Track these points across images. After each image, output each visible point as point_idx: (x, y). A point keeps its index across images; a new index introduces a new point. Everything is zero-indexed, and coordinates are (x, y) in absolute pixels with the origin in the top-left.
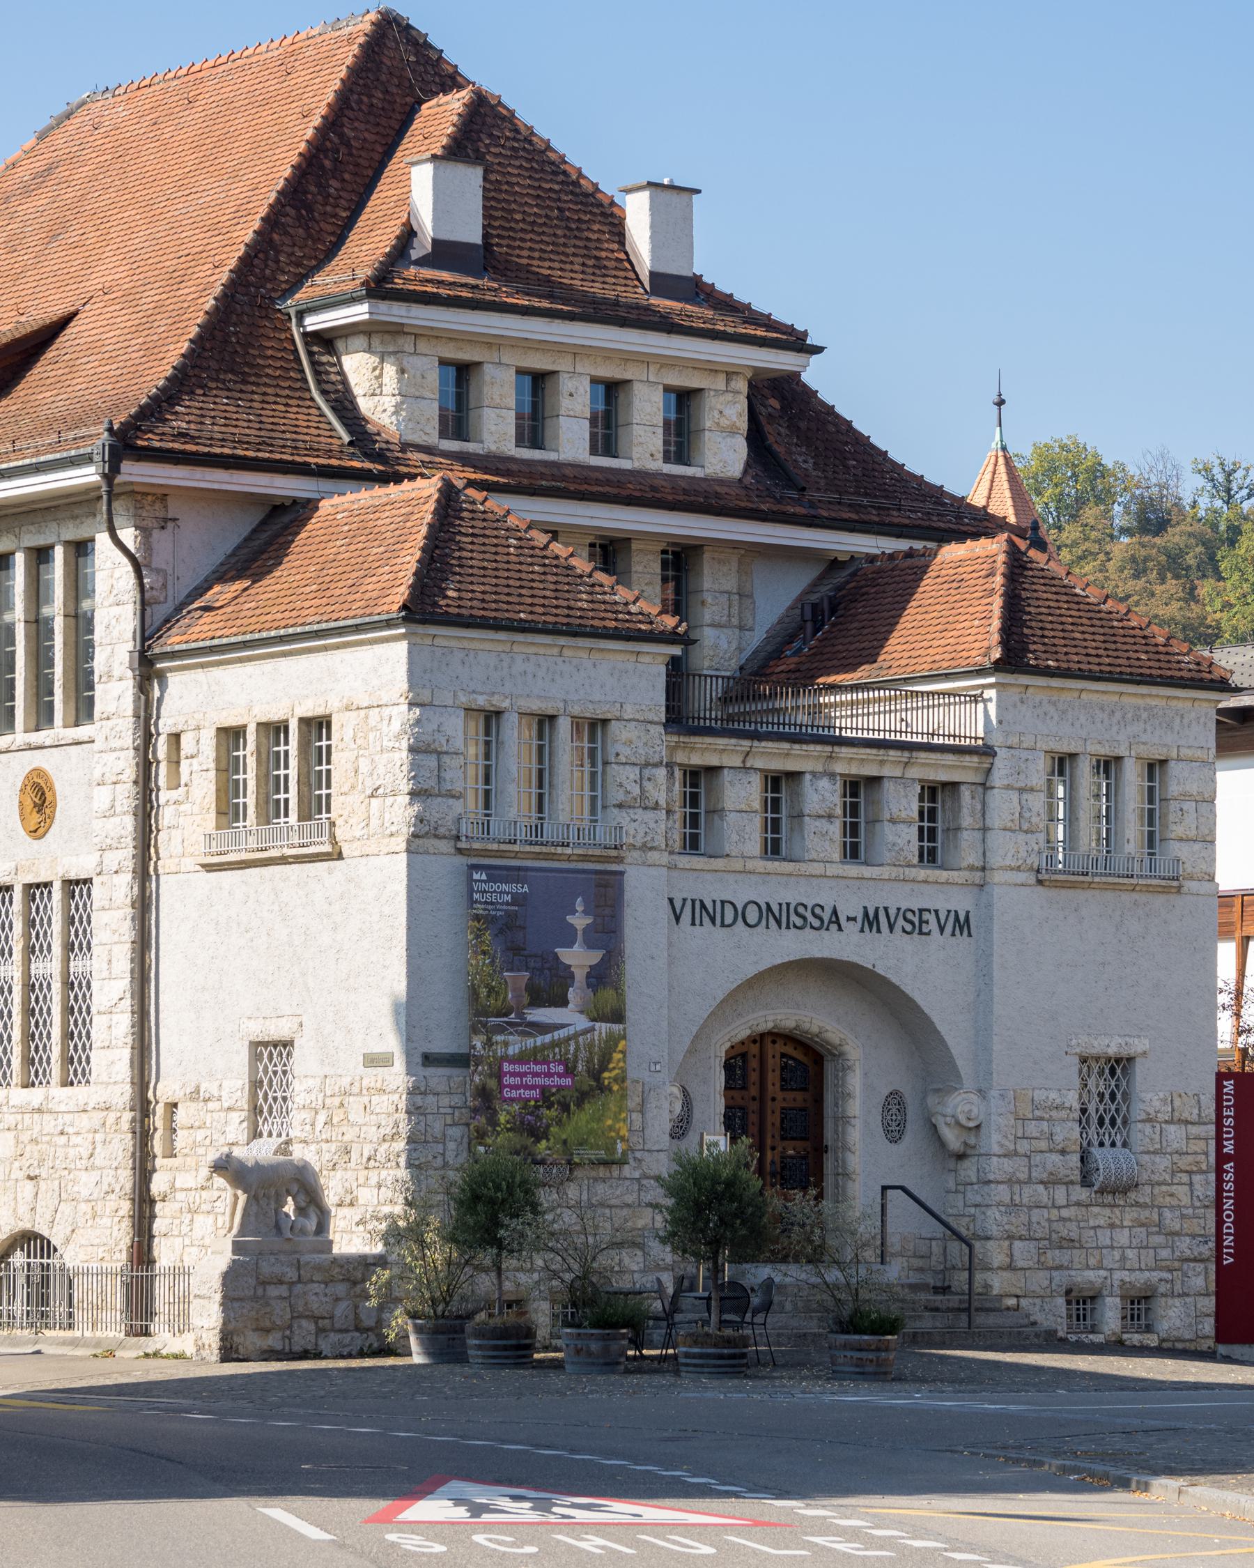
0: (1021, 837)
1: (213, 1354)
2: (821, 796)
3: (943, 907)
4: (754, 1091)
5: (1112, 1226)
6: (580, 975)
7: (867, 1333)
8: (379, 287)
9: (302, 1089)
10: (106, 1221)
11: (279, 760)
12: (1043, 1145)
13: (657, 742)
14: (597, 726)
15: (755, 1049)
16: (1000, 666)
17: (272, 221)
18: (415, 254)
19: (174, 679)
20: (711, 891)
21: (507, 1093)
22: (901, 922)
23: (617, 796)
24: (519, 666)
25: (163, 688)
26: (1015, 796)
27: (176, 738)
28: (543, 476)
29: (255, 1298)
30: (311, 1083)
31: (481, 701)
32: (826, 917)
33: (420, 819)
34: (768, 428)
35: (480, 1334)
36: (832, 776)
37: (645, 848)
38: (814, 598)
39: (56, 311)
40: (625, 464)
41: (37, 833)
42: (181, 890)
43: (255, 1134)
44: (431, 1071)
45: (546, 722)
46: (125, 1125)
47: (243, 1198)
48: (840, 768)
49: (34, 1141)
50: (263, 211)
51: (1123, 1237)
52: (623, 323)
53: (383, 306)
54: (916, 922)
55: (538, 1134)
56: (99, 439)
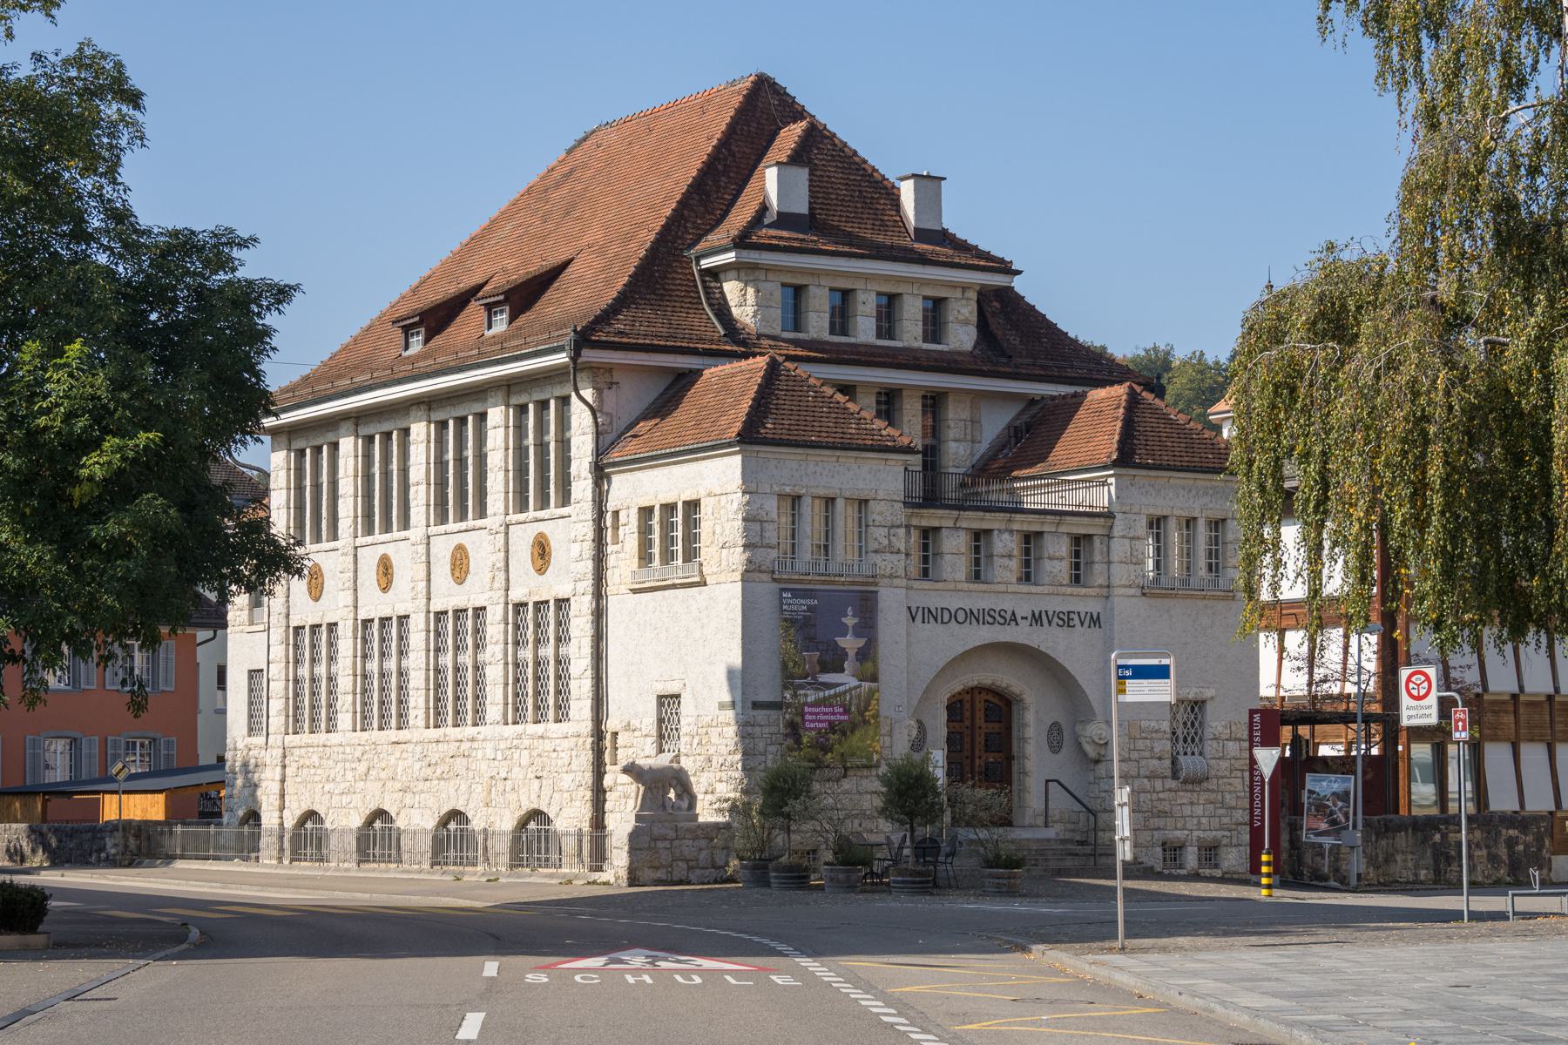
0: (1132, 567)
1: (624, 882)
2: (1005, 544)
3: (1082, 610)
4: (967, 723)
5: (1192, 804)
6: (851, 654)
7: (1006, 870)
8: (742, 242)
9: (687, 723)
10: (578, 803)
11: (672, 526)
12: (1147, 754)
13: (900, 514)
14: (863, 503)
15: (968, 697)
16: (1115, 464)
17: (684, 203)
18: (766, 221)
19: (615, 478)
20: (935, 601)
21: (808, 725)
22: (1056, 619)
23: (873, 545)
24: (811, 468)
25: (609, 484)
26: (1127, 542)
27: (616, 513)
28: (845, 352)
29: (649, 848)
30: (690, 720)
31: (788, 490)
32: (1008, 617)
33: (749, 561)
34: (991, 320)
35: (776, 870)
36: (1011, 532)
37: (891, 576)
38: (1018, 423)
39: (554, 259)
40: (899, 344)
41: (541, 571)
42: (619, 605)
43: (661, 751)
44: (756, 712)
45: (830, 501)
46: (588, 746)
47: (642, 789)
48: (1016, 527)
49: (539, 755)
50: (678, 197)
51: (1199, 810)
52: (895, 259)
53: (745, 253)
54: (1066, 620)
55: (826, 749)
56: (568, 337)
